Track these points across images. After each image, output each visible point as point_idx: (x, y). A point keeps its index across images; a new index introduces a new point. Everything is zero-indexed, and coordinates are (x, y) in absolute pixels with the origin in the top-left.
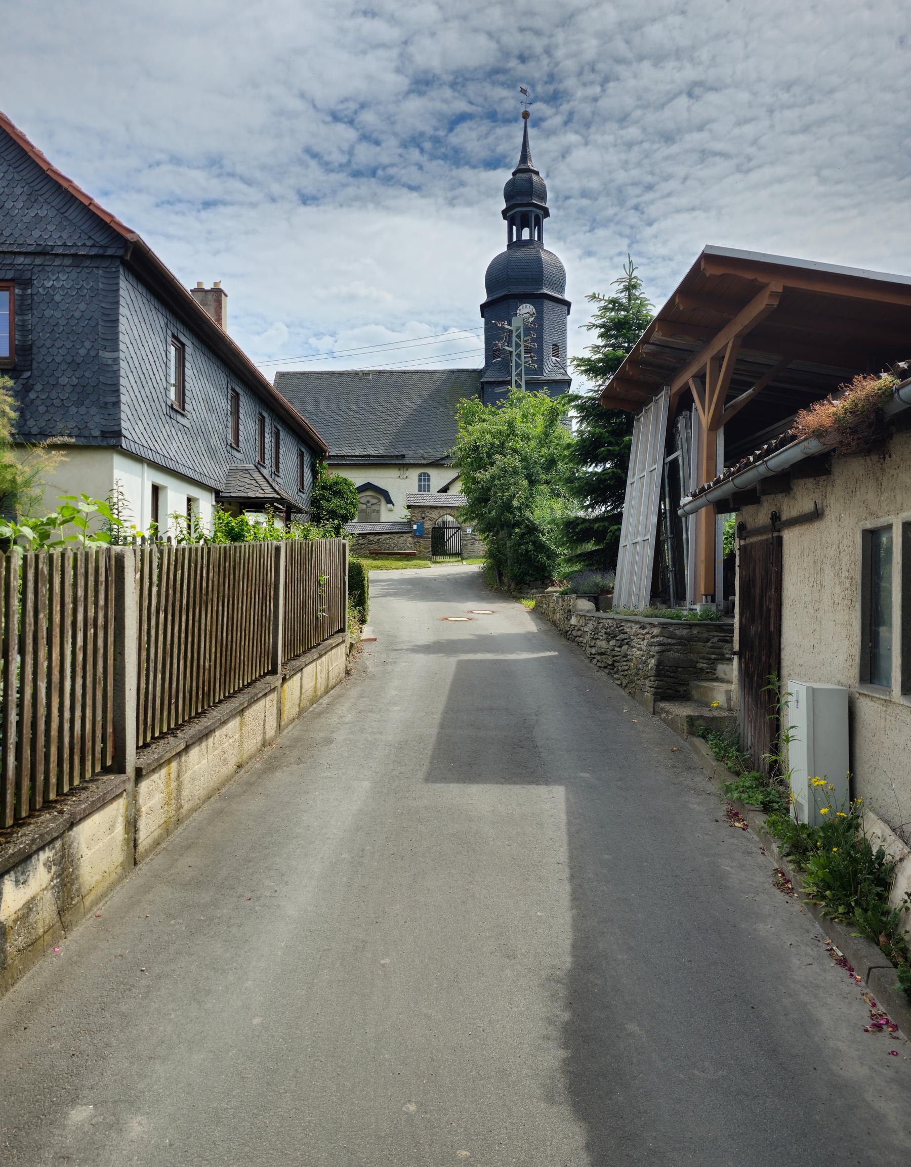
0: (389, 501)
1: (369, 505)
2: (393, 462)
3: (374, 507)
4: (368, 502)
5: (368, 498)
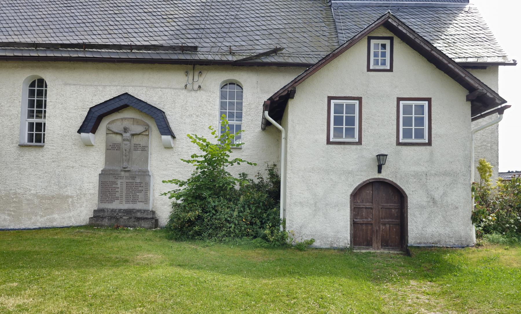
0: (166, 129)
1: (127, 135)
2: (174, 57)
3: (136, 140)
4: (126, 130)
5: (126, 124)
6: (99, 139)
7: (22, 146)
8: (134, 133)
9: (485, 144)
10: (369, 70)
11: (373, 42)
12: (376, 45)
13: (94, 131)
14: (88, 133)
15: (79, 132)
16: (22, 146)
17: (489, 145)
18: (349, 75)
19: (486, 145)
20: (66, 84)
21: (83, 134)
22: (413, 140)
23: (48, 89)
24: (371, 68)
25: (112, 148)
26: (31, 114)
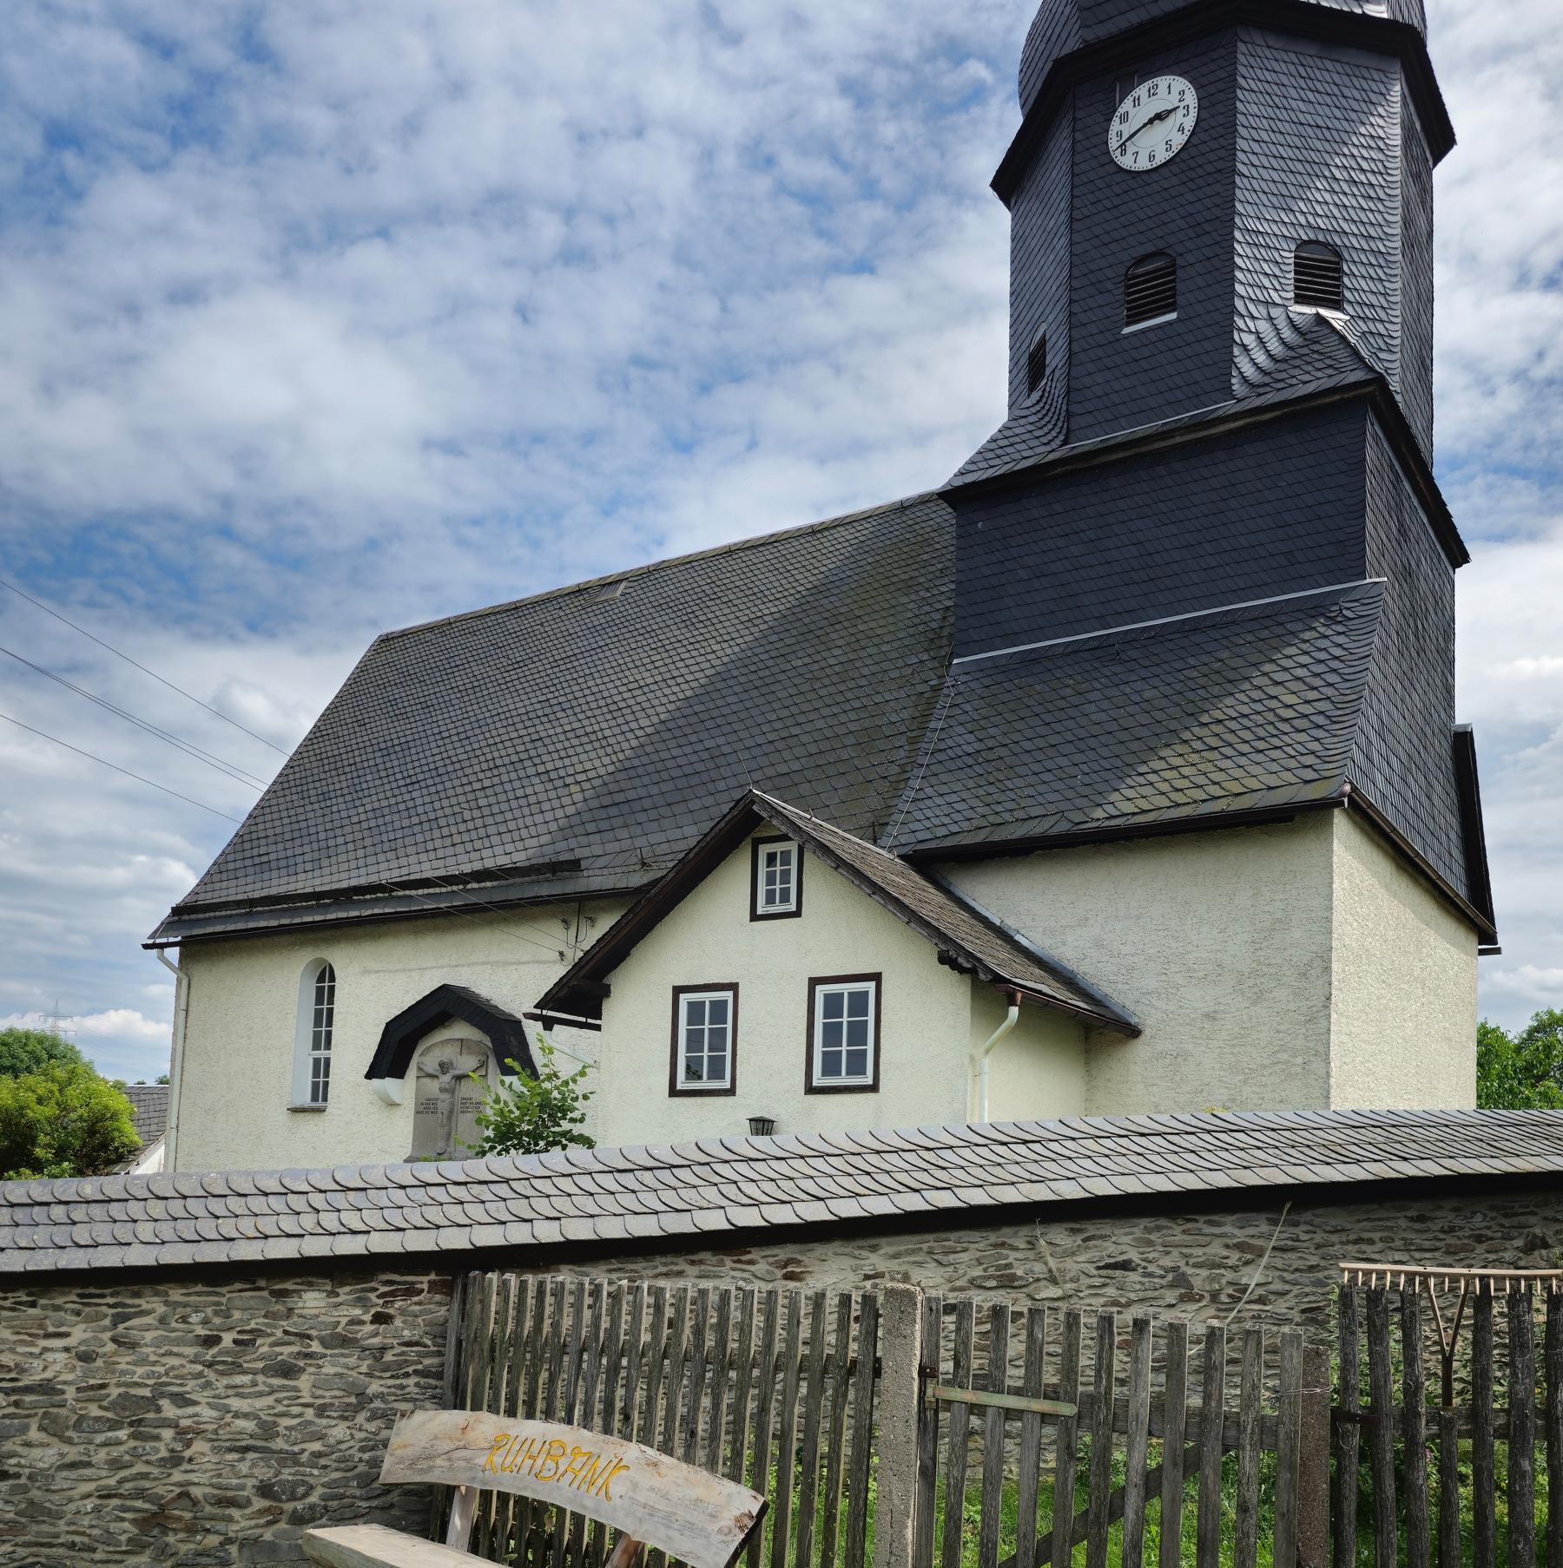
6: (403, 1090)
7: (295, 1110)
8: (457, 1072)
9: (1285, 1057)
10: (755, 917)
11: (764, 850)
12: (771, 859)
13: (399, 1072)
14: (383, 1077)
15: (369, 1076)
16: (295, 1110)
17: (1299, 1060)
18: (720, 935)
19: (1287, 1062)
20: (366, 972)
21: (375, 1082)
22: (843, 1080)
23: (337, 984)
24: (760, 911)
25: (425, 1108)
26: (316, 1046)
